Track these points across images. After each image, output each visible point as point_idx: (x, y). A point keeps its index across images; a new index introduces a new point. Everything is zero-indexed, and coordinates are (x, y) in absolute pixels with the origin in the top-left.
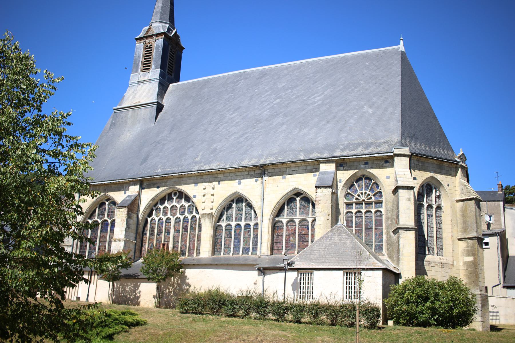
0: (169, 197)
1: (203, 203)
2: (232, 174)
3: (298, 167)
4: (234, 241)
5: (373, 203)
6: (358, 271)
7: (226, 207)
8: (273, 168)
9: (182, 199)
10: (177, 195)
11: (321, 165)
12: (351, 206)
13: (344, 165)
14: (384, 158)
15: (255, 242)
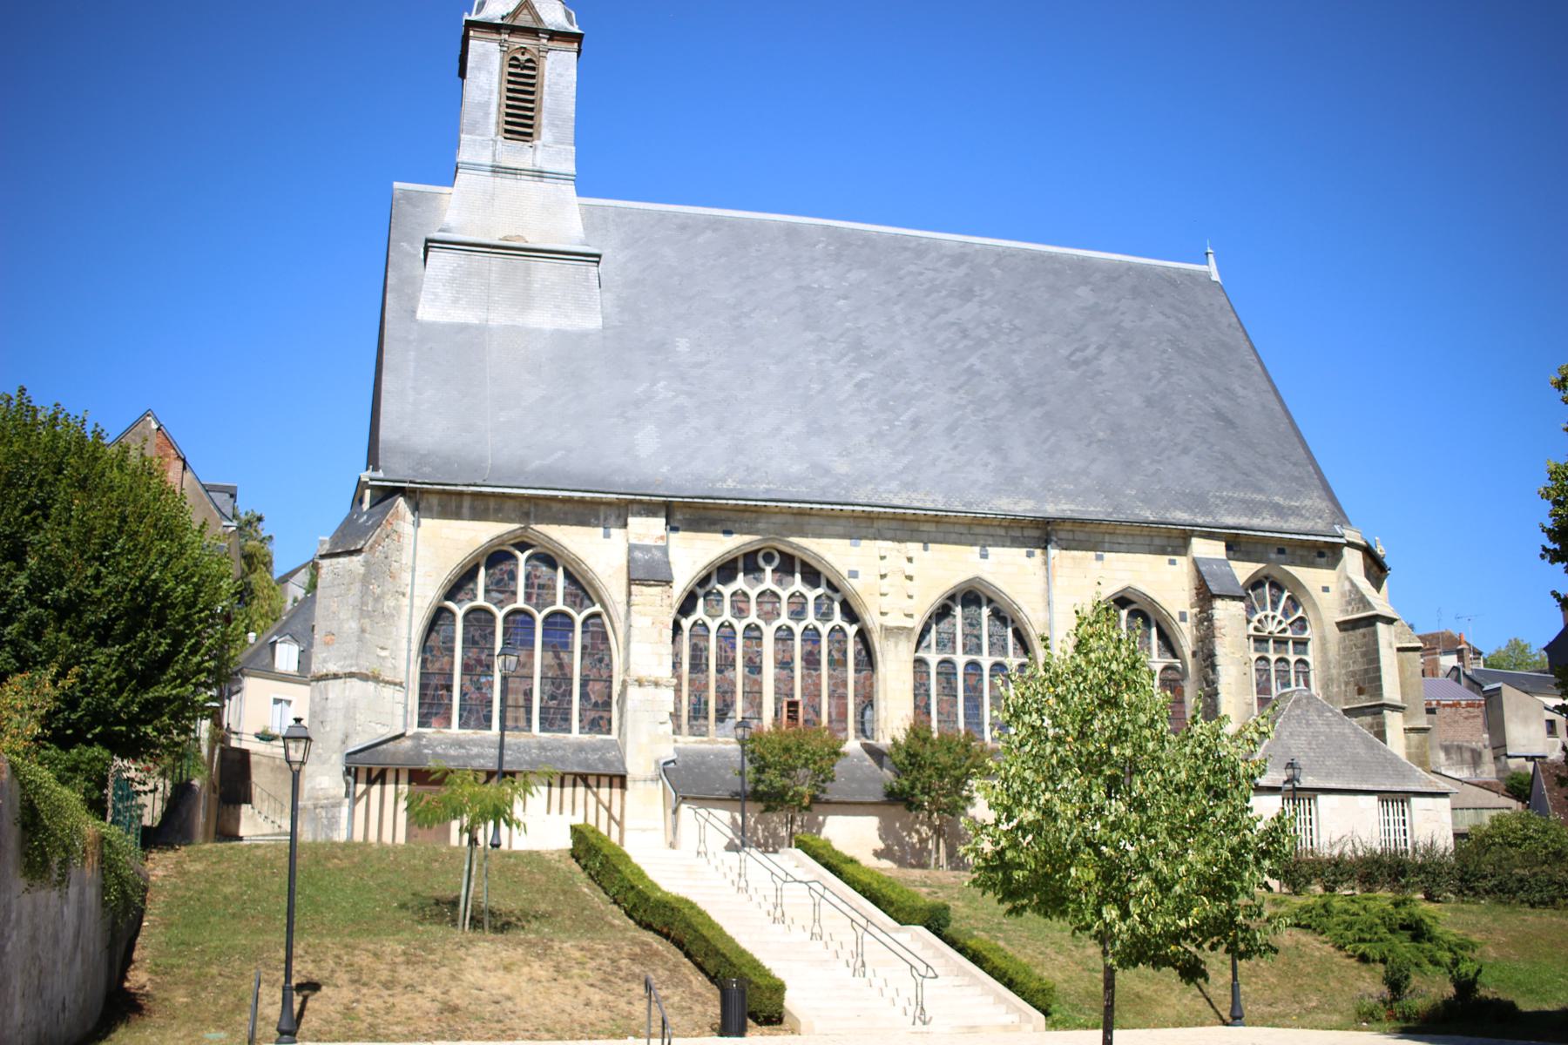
0: (749, 563)
3: (1132, 535)
5: (1290, 643)
6: (1403, 797)
9: (792, 574)
10: (776, 562)
11: (1195, 541)
12: (1283, 646)
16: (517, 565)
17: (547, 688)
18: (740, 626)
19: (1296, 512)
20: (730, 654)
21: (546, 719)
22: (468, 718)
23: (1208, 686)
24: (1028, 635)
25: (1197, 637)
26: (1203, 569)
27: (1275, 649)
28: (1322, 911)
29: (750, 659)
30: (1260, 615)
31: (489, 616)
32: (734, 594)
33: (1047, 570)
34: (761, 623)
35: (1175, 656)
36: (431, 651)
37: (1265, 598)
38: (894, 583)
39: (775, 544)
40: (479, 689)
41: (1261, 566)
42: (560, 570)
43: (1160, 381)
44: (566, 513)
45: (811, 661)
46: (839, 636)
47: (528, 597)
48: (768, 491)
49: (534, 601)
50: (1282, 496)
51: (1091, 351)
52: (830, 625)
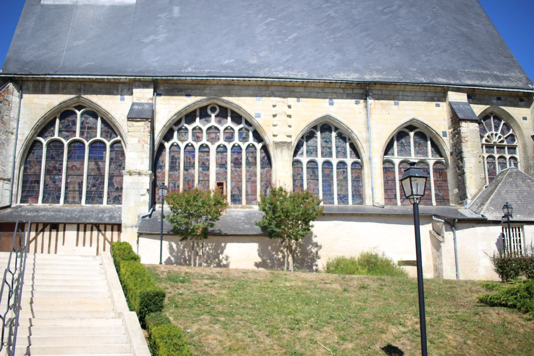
1: (274, 126)
2: (319, 90)
3: (415, 91)
4: (323, 185)
5: (506, 148)
7: (305, 135)
8: (381, 88)
9: (226, 117)
12: (502, 150)
13: (473, 98)
14: (520, 95)
15: (355, 188)
16: (76, 117)
17: (91, 181)
18: (197, 146)
19: (507, 79)
20: (192, 160)
21: (90, 197)
22: (48, 198)
23: (459, 170)
24: (358, 146)
25: (453, 144)
26: (454, 107)
27: (498, 152)
28: (526, 294)
29: (203, 163)
30: (489, 133)
31: (61, 144)
32: (194, 129)
33: (367, 110)
34: (209, 144)
35: (441, 156)
36: (30, 163)
37: (491, 125)
38: (281, 119)
39: (215, 101)
40: (54, 182)
41: (487, 106)
42: (99, 119)
43: (431, 21)
44: (100, 89)
45: (237, 163)
46: (252, 149)
47: (82, 134)
48: (209, 72)
49: (85, 135)
50: (498, 71)
51: (395, 7)
52: (247, 144)
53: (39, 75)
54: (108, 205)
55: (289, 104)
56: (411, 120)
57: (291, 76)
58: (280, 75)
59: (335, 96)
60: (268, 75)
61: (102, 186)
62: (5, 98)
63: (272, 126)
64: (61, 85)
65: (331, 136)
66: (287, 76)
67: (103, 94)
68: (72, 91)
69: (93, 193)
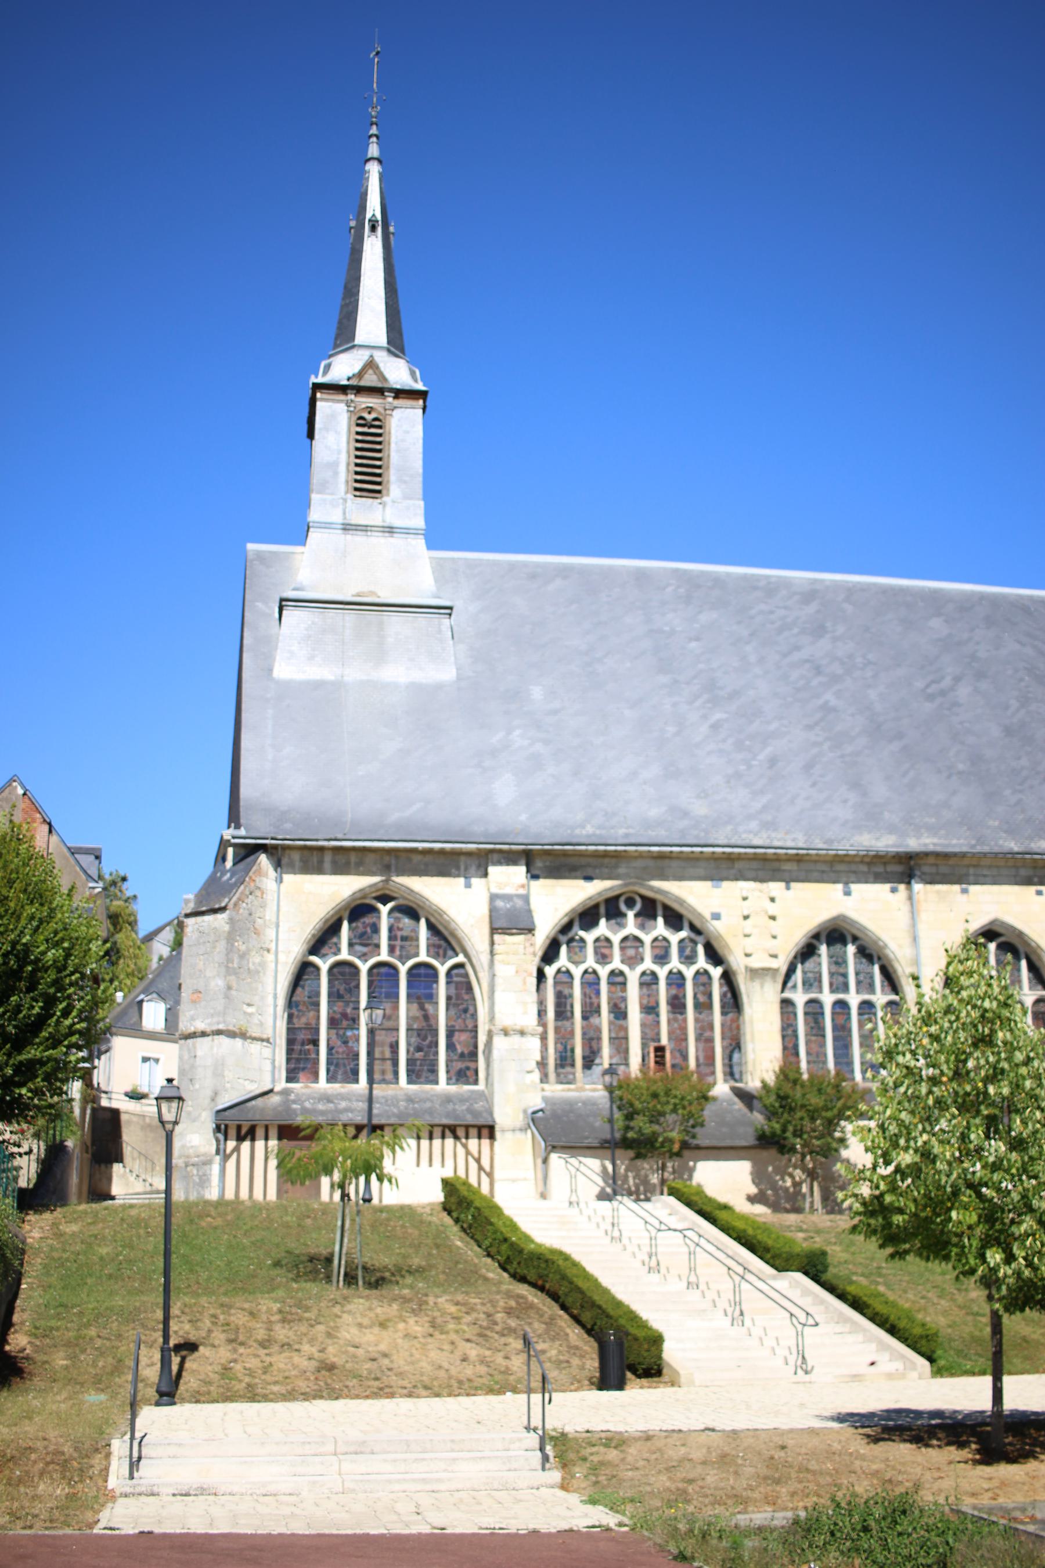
2: (824, 867)
3: (998, 867)
9: (654, 917)
16: (379, 918)
18: (604, 972)
20: (595, 1000)
22: (336, 1072)
32: (597, 940)
33: (912, 905)
34: (625, 968)
36: (297, 1006)
40: (345, 1043)
44: (426, 865)
45: (677, 1005)
46: (704, 979)
47: (392, 950)
48: (627, 835)
49: (398, 952)
51: (947, 682)
53: (317, 840)
54: (449, 1087)
55: (773, 895)
56: (993, 922)
57: (776, 843)
58: (756, 842)
59: (853, 877)
60: (733, 842)
61: (433, 1049)
62: (258, 884)
63: (741, 936)
64: (353, 858)
65: (845, 952)
66: (767, 843)
67: (432, 876)
68: (374, 869)
69: (418, 1063)
